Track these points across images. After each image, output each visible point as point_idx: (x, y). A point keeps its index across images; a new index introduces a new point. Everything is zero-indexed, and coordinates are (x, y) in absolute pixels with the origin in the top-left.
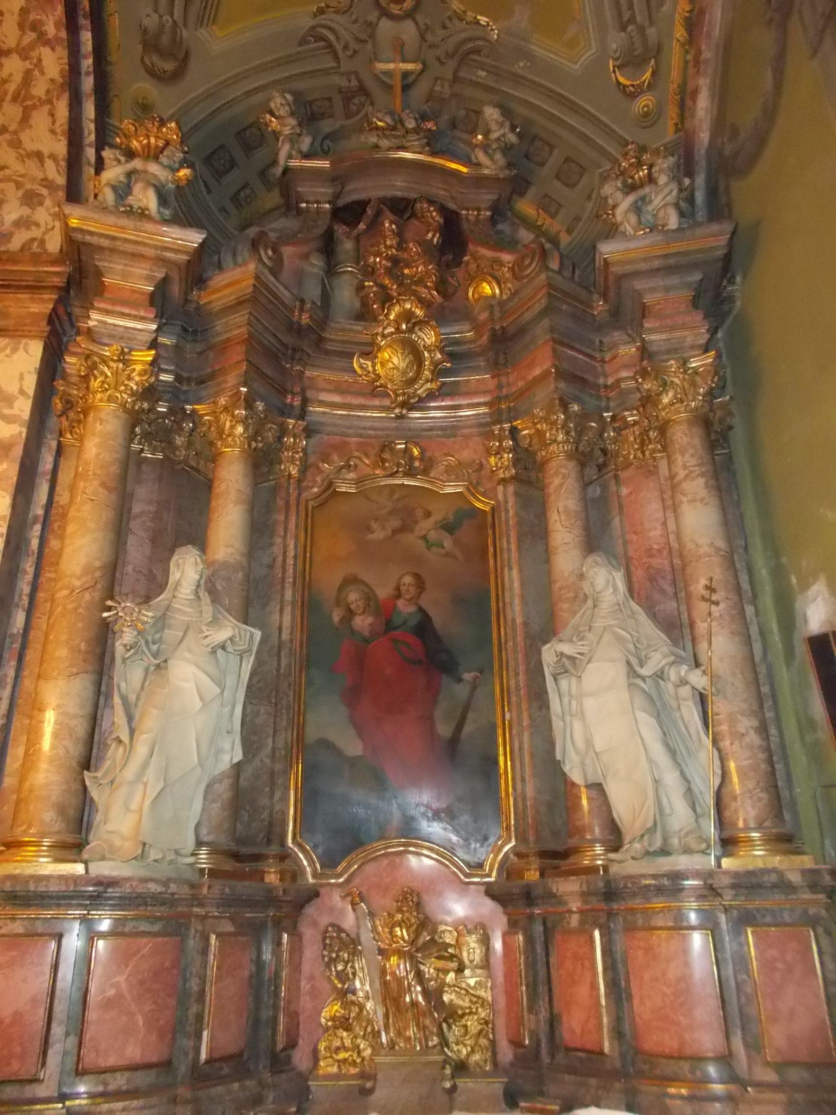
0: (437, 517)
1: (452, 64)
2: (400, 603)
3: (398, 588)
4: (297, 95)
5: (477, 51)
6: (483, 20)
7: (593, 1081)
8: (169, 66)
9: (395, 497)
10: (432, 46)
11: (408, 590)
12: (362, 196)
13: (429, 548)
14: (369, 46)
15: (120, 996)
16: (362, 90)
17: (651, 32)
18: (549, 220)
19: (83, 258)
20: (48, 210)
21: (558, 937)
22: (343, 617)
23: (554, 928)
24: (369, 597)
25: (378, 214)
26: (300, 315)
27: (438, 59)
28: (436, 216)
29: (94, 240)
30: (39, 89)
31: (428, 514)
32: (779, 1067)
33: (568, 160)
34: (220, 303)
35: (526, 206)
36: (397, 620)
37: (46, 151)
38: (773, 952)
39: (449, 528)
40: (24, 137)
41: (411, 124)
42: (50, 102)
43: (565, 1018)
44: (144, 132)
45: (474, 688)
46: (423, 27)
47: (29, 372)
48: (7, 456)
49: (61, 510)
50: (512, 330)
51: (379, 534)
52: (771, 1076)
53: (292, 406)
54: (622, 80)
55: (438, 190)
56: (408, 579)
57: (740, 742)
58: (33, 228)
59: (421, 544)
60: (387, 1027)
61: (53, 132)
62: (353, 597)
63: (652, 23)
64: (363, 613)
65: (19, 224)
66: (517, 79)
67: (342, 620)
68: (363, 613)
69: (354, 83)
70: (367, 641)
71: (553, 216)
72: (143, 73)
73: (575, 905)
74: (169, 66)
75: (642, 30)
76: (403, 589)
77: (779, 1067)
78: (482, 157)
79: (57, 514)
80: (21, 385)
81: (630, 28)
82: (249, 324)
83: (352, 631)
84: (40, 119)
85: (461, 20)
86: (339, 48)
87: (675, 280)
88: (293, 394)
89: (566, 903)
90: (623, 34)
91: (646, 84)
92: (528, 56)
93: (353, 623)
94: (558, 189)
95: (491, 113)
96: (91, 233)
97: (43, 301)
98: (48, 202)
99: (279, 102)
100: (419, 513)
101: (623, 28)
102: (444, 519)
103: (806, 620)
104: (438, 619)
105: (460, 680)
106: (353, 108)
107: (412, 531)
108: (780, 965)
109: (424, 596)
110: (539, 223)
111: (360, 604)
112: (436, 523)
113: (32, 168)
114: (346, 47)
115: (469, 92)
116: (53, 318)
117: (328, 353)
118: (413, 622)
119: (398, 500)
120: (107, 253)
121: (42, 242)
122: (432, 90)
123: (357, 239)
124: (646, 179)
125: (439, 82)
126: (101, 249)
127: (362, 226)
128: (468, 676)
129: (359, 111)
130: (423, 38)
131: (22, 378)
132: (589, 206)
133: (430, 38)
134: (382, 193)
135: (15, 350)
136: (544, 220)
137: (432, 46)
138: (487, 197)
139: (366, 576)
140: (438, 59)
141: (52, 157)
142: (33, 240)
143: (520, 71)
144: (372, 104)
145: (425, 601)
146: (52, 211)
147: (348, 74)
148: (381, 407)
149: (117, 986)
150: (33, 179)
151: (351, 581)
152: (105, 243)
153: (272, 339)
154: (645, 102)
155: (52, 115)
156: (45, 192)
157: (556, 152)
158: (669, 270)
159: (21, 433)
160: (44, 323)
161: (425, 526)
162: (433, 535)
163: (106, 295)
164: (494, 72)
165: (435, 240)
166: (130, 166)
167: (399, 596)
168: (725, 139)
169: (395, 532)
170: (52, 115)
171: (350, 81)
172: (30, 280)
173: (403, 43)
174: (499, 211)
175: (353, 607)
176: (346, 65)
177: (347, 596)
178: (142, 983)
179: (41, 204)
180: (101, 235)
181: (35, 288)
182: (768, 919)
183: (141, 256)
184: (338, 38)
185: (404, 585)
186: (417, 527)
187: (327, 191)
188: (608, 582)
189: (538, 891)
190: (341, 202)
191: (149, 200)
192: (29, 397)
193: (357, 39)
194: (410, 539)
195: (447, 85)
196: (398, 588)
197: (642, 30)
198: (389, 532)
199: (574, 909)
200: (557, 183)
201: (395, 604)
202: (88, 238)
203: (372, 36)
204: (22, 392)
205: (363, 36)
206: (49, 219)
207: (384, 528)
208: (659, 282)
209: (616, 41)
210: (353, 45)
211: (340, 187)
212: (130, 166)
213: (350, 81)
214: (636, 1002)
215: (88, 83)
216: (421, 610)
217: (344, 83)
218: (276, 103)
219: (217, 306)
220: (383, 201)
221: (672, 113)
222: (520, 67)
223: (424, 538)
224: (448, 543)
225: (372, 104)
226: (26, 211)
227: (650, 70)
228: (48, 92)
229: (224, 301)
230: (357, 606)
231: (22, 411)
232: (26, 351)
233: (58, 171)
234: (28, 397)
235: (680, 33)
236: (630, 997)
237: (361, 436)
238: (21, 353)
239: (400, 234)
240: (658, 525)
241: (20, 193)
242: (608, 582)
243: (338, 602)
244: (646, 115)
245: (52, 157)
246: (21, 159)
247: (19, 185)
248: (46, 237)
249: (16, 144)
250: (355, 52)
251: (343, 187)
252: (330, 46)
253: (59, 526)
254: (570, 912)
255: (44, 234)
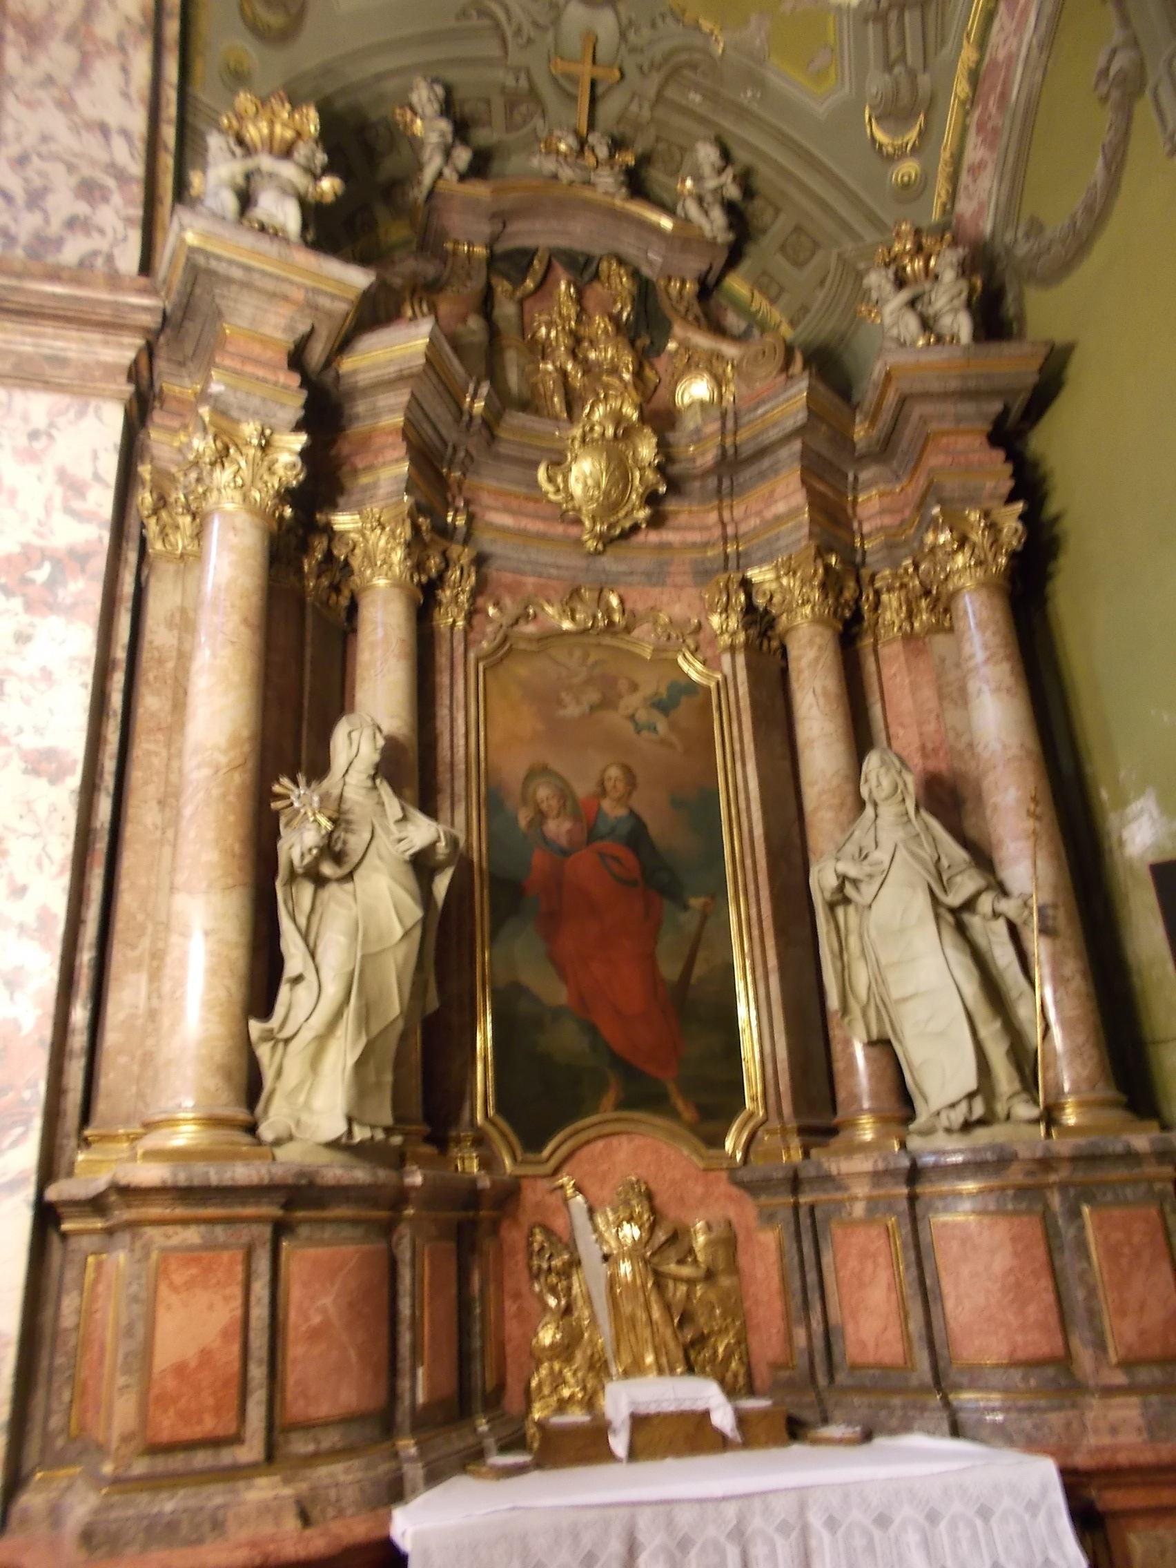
0: (647, 690)
1: (656, 79)
2: (606, 804)
3: (602, 783)
4: (449, 90)
5: (694, 67)
6: (706, 25)
7: (896, 1401)
8: (274, 19)
9: (591, 660)
10: (633, 50)
11: (615, 787)
12: (527, 242)
13: (638, 732)
14: (550, 36)
15: (326, 1325)
16: (533, 94)
17: (924, 80)
18: (765, 305)
19: (198, 291)
20: (117, 212)
21: (837, 1231)
22: (532, 820)
23: (827, 1220)
24: (565, 794)
25: (549, 268)
26: (473, 401)
27: (641, 68)
28: (625, 282)
29: (221, 268)
30: (106, 27)
31: (634, 687)
32: (1127, 1364)
33: (798, 229)
34: (372, 374)
35: (737, 284)
36: (602, 828)
37: (113, 121)
38: (1118, 1236)
39: (663, 706)
40: (82, 98)
41: (603, 152)
42: (123, 50)
43: (850, 1329)
44: (269, 115)
45: (704, 918)
46: (625, 21)
47: (106, 450)
48: (83, 570)
49: (156, 654)
50: (746, 451)
51: (572, 710)
52: (1120, 1378)
53: (455, 528)
54: (880, 136)
55: (629, 246)
56: (614, 772)
57: (1066, 988)
58: (95, 235)
59: (630, 727)
60: (617, 1352)
61: (125, 95)
62: (543, 793)
63: (925, 67)
64: (558, 815)
65: (72, 223)
66: (742, 113)
67: (530, 824)
68: (558, 815)
69: (523, 83)
70: (565, 853)
71: (773, 301)
72: (240, 25)
73: (861, 1190)
74: (274, 19)
75: (912, 75)
76: (609, 785)
77: (1127, 1364)
78: (693, 210)
79: (152, 658)
80: (96, 468)
81: (898, 69)
82: (409, 408)
83: (544, 838)
84: (106, 73)
85: (678, 20)
86: (509, 34)
87: (968, 408)
88: (456, 511)
89: (846, 1189)
90: (887, 76)
91: (909, 146)
92: (759, 83)
93: (545, 828)
94: (779, 264)
95: (707, 154)
96: (219, 258)
97: (121, 346)
98: (116, 199)
99: (424, 96)
100: (623, 685)
101: (888, 67)
102: (656, 694)
103: (1121, 843)
104: (655, 828)
105: (686, 907)
106: (517, 118)
107: (616, 708)
108: (1126, 1250)
109: (635, 795)
110: (754, 309)
111: (554, 803)
112: (645, 699)
113: (92, 144)
114: (518, 32)
115: (679, 121)
116: (133, 374)
117: (498, 457)
118: (624, 829)
119: (596, 664)
120: (234, 288)
121: (110, 259)
122: (626, 109)
123: (521, 303)
124: (923, 274)
125: (636, 100)
126: (229, 281)
127: (530, 284)
128: (696, 902)
129: (525, 122)
130: (623, 36)
131: (95, 456)
132: (821, 295)
133: (632, 36)
134: (561, 242)
135: (81, 414)
136: (760, 304)
137: (633, 50)
138: (694, 265)
139: (556, 765)
140: (641, 68)
141: (125, 133)
142: (95, 253)
143: (745, 102)
144: (544, 115)
145: (639, 802)
146: (124, 212)
147: (516, 71)
148: (854, 565)
149: (323, 1310)
150: (93, 162)
151: (539, 771)
152: (237, 273)
153: (430, 431)
154: (909, 168)
155: (125, 70)
156: (111, 183)
157: (782, 217)
158: (965, 395)
159: (100, 539)
160: (123, 379)
161: (632, 702)
162: (642, 715)
163: (230, 348)
164: (712, 97)
165: (625, 315)
166: (251, 163)
167: (603, 792)
168: (1020, 234)
169: (593, 708)
170: (125, 70)
171: (517, 80)
172: (106, 314)
173: (597, 39)
174: (707, 289)
175: (544, 806)
176: (516, 56)
177: (535, 793)
178: (351, 1305)
179: (105, 199)
180: (231, 262)
181: (111, 326)
182: (1110, 1197)
183: (286, 298)
184: (509, 19)
185: (610, 779)
186: (622, 704)
187: (486, 229)
188: (896, 787)
189: (808, 1171)
190: (500, 248)
191: (289, 217)
192: (107, 486)
193: (536, 24)
194: (615, 719)
195: (646, 106)
196: (602, 783)
197: (912, 75)
198: (586, 708)
199: (860, 1195)
200: (779, 258)
201: (599, 808)
202: (214, 264)
203: (556, 22)
204: (97, 477)
205: (542, 20)
206: (120, 226)
207: (578, 702)
208: (949, 408)
209: (877, 83)
210: (528, 29)
211: (501, 225)
212: (251, 163)
213: (517, 80)
214: (950, 1304)
215: (172, 28)
216: (632, 813)
217: (510, 81)
218: (420, 96)
219: (363, 379)
220: (556, 255)
221: (941, 189)
222: (747, 96)
223: (632, 717)
224: (662, 726)
225: (544, 115)
226: (82, 208)
227: (917, 128)
228: (121, 36)
229: (379, 373)
230: (549, 806)
231: (100, 506)
232: (100, 419)
233: (132, 155)
234: (107, 486)
235: (961, 87)
236: (940, 1297)
237: (540, 576)
238: (89, 421)
239: (579, 299)
240: (932, 717)
241: (73, 181)
242: (896, 787)
243: (524, 801)
244: (906, 186)
245: (125, 133)
246: (75, 129)
247: (71, 168)
248: (116, 252)
249: (67, 105)
250: (530, 41)
251: (504, 226)
252: (497, 26)
253: (156, 678)
254: (854, 1199)
255: (112, 246)
